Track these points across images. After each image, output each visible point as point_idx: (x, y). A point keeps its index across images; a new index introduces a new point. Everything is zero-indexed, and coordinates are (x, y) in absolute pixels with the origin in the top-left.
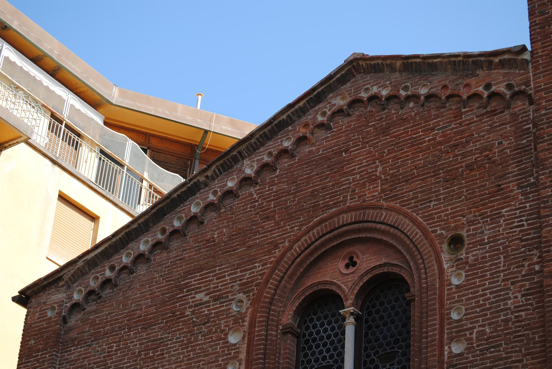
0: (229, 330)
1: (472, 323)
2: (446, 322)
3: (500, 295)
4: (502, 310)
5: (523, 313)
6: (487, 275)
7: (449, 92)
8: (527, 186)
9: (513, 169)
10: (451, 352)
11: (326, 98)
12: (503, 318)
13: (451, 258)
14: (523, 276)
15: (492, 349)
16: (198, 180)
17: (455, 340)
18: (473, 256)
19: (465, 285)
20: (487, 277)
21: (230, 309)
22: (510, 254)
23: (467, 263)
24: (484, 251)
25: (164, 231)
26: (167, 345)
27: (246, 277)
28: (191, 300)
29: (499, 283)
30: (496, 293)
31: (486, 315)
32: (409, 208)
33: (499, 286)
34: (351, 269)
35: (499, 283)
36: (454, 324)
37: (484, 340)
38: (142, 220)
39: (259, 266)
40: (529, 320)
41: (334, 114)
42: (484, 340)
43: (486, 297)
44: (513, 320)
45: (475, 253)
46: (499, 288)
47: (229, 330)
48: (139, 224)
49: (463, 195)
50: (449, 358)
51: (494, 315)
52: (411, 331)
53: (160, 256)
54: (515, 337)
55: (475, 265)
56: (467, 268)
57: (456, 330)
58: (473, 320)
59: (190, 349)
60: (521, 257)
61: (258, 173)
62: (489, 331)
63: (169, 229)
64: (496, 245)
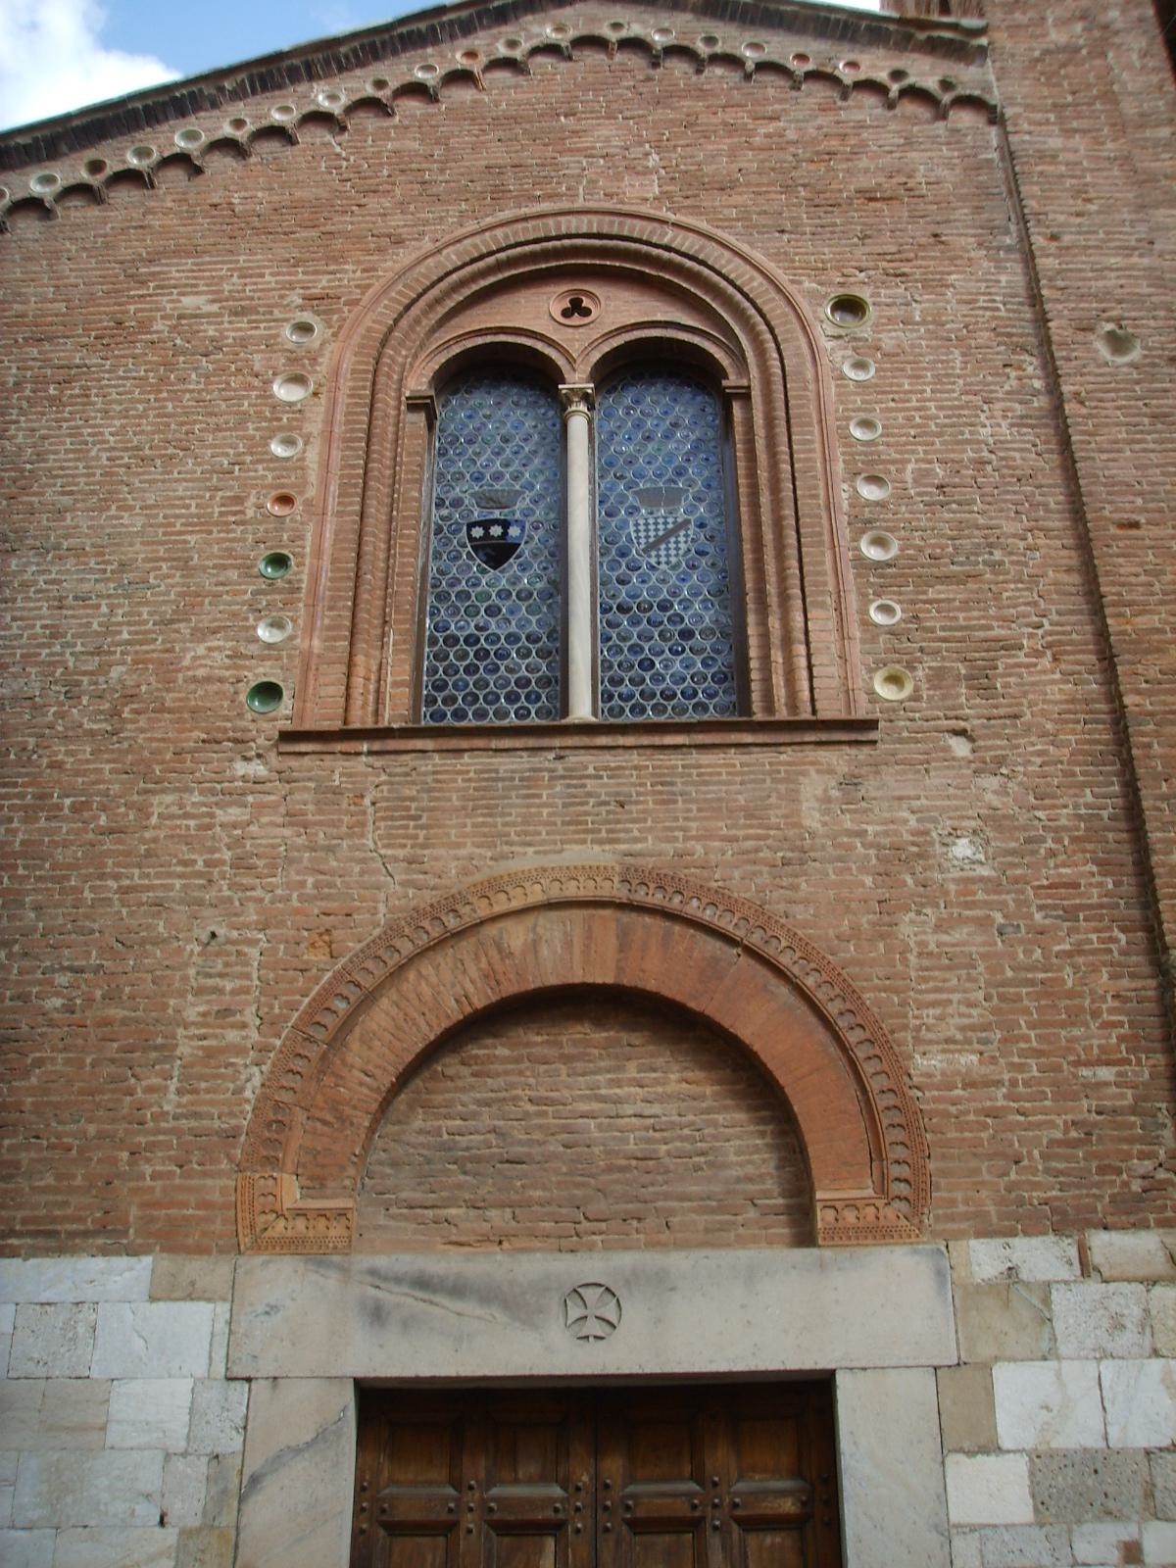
0: (275, 374)
1: (901, 453)
3: (960, 416)
4: (968, 442)
7: (810, 66)
8: (999, 249)
9: (963, 213)
11: (517, 18)
14: (1008, 393)
16: (200, 90)
18: (891, 338)
19: (876, 385)
21: (278, 335)
23: (878, 349)
25: (96, 167)
26: (99, 380)
28: (169, 306)
33: (956, 399)
34: (576, 320)
38: (47, 132)
39: (354, 272)
41: (536, 51)
42: (932, 485)
47: (275, 374)
48: (36, 140)
53: (77, 211)
55: (898, 355)
59: (165, 395)
61: (350, 110)
63: (112, 167)
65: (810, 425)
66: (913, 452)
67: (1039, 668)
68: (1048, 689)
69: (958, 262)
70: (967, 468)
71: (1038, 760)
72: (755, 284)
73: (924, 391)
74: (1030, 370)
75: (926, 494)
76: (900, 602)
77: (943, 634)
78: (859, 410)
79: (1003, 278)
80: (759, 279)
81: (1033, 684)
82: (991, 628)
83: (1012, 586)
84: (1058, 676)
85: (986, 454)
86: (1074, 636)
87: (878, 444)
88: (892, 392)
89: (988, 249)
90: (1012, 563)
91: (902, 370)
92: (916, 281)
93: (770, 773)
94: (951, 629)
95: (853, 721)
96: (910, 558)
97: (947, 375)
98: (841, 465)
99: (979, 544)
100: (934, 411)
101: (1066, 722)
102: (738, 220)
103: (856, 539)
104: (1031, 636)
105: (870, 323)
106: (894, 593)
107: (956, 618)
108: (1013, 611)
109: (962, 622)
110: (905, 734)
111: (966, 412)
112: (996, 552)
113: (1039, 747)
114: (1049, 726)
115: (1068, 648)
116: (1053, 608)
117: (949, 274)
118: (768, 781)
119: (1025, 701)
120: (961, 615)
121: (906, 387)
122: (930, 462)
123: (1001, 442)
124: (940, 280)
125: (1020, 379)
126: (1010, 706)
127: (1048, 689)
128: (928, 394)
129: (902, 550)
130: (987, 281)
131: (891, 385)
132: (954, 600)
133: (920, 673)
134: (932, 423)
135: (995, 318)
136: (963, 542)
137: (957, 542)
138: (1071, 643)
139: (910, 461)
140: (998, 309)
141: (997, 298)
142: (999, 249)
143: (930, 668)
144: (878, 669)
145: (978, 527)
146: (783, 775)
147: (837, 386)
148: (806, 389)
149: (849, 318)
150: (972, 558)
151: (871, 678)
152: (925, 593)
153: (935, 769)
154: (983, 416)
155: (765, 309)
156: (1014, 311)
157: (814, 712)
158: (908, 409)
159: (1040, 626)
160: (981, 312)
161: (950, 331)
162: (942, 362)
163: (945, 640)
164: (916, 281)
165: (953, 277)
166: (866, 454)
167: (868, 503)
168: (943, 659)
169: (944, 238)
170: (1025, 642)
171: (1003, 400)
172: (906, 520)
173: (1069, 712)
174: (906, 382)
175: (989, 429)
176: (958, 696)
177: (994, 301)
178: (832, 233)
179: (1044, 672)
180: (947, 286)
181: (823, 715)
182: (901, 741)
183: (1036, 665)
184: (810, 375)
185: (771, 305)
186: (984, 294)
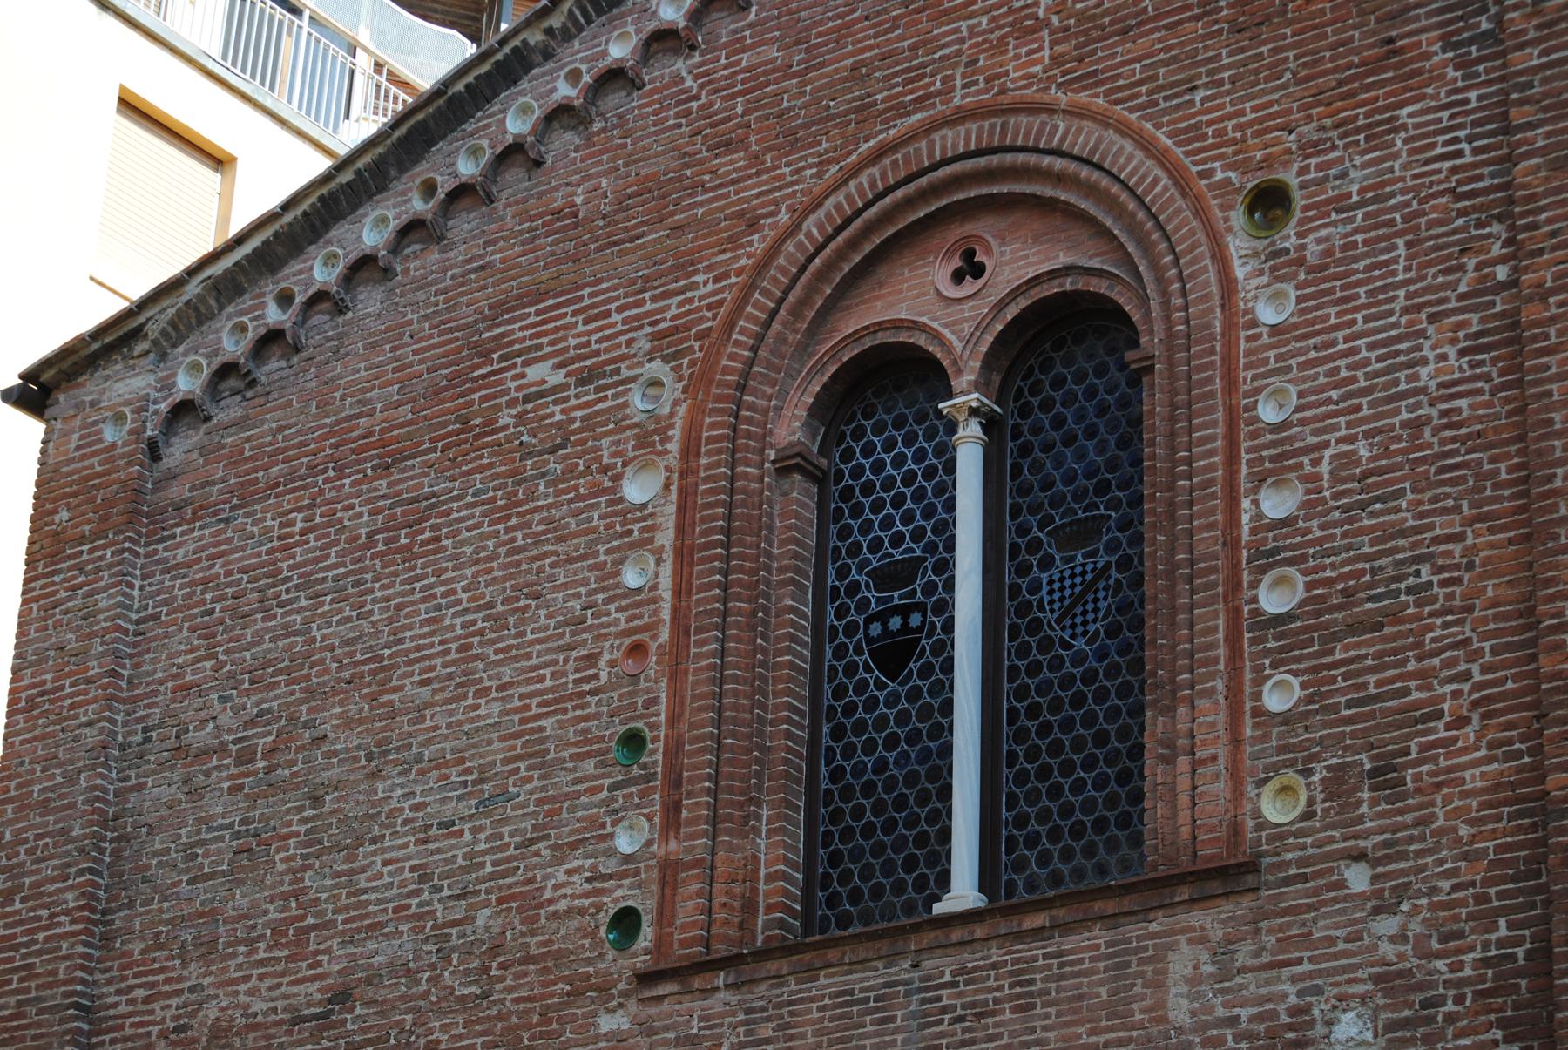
3: (1397, 353)
4: (1403, 395)
8: (1471, 41)
10: (1259, 516)
14: (1462, 297)
17: (1270, 480)
23: (1300, 262)
24: (1349, 228)
30: (1385, 346)
31: (1358, 408)
32: (1131, 110)
44: (1435, 422)
45: (1323, 233)
46: (1393, 333)
50: (1253, 531)
54: (1441, 470)
56: (1302, 276)
57: (1272, 452)
67: (1460, 744)
71: (1446, 885)
76: (1295, 673)
83: (1439, 621)
86: (1510, 685)
119: (1439, 799)
127: (1467, 775)
132: (1365, 657)
133: (1316, 778)
137: (1377, 564)
138: (1503, 696)
139: (1326, 444)
143: (1328, 768)
146: (1150, 952)
151: (1258, 795)
170: (1446, 706)
175: (1432, 367)
176: (1360, 803)
182: (1288, 881)
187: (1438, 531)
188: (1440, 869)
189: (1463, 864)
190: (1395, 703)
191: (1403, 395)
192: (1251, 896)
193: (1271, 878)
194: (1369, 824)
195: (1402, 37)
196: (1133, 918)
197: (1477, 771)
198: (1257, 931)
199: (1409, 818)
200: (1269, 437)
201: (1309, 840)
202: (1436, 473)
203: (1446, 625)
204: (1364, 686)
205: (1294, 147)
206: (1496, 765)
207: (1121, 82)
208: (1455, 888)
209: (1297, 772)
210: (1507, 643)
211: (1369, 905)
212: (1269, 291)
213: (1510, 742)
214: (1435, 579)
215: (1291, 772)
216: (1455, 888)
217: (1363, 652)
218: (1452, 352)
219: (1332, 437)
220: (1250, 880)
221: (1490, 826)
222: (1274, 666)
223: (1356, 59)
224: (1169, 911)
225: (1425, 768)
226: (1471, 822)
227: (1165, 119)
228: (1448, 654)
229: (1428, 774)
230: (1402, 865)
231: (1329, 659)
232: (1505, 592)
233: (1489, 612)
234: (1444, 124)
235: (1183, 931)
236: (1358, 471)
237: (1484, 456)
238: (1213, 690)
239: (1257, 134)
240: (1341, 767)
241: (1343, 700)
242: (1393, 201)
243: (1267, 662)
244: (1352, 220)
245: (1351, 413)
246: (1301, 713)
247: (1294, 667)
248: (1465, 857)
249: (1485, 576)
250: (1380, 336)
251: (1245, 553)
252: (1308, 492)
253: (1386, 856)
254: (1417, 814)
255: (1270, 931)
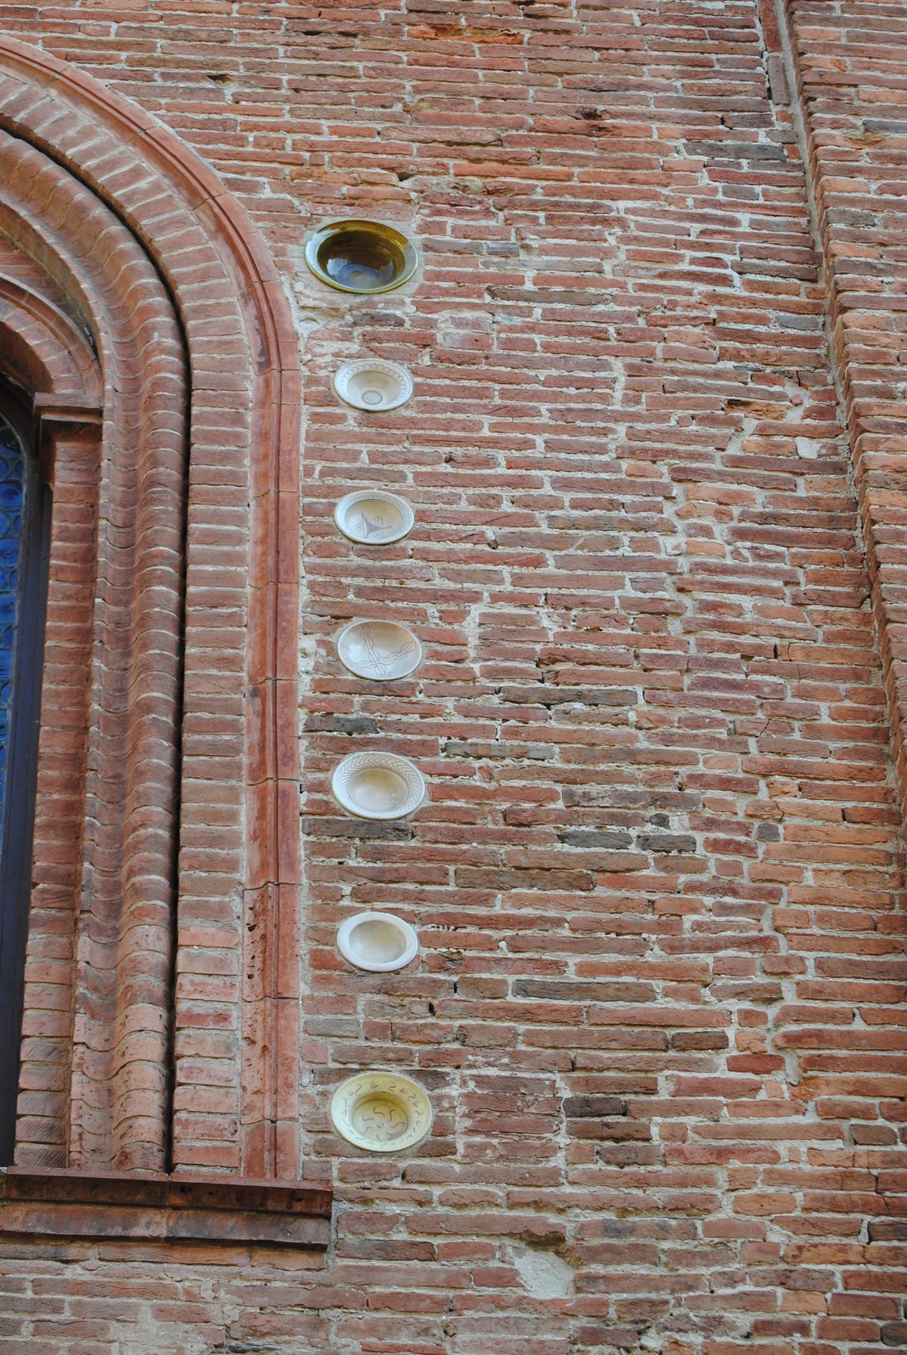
2: (302, 541)
3: (613, 505)
4: (626, 564)
5: (747, 602)
6: (493, 427)
8: (740, 152)
10: (334, 663)
12: (630, 592)
13: (333, 302)
14: (736, 462)
15: (578, 706)
17: (356, 621)
18: (460, 324)
20: (536, 421)
22: (658, 364)
23: (425, 343)
24: (517, 321)
27: (415, 30)
29: (605, 458)
30: (590, 489)
31: (538, 562)
32: (97, 73)
33: (605, 467)
35: (605, 458)
36: (353, 557)
37: (529, 659)
40: (782, 637)
42: (528, 656)
43: (535, 492)
44: (689, 614)
45: (468, 315)
46: (604, 476)
49: (400, 100)
50: (321, 687)
51: (579, 572)
52: (52, 552)
54: (706, 684)
55: (473, 360)
56: (426, 361)
57: (360, 581)
58: (464, 567)
60: (720, 390)
62: (557, 629)
64: (582, 313)
65: (237, 499)
66: (488, 577)
67: (762, 1095)
68: (782, 1147)
69: (639, 173)
70: (620, 622)
71: (745, 1320)
72: (143, 184)
73: (531, 444)
74: (794, 417)
75: (509, 673)
76: (411, 918)
77: (521, 1000)
78: (362, 473)
79: (745, 218)
80: (155, 175)
81: (743, 1133)
82: (647, 995)
83: (709, 901)
84: (810, 1119)
85: (668, 594)
86: (859, 1025)
87: (401, 554)
88: (448, 442)
89: (712, 150)
90: (716, 846)
91: (480, 394)
92: (535, 206)
93: (34, 1307)
94: (544, 991)
95: (266, 1192)
96: (451, 815)
97: (588, 414)
98: (304, 595)
99: (633, 798)
100: (548, 489)
101: (821, 1228)
102: (120, 46)
103: (323, 765)
104: (748, 1017)
105: (412, 288)
106: (406, 896)
107: (557, 967)
108: (707, 959)
109: (572, 976)
110: (401, 1235)
111: (627, 499)
112: (674, 820)
113: (748, 1287)
114: (777, 1236)
115: (843, 1053)
116: (810, 957)
117: (615, 196)
118: (26, 1330)
119: (721, 1175)
120: (573, 960)
121: (486, 432)
122: (526, 602)
123: (709, 569)
124: (592, 208)
125: (762, 432)
126: (682, 1183)
127: (782, 1147)
128: (539, 451)
129: (437, 793)
130: (703, 218)
131: (448, 425)
132: (558, 922)
133: (454, 1091)
134: (540, 515)
135: (715, 298)
136: (593, 788)
137: (579, 789)
138: (850, 1040)
139: (475, 597)
140: (725, 281)
141: (727, 258)
142: (740, 152)
143: (481, 1081)
144: (342, 1075)
145: (633, 757)
146: (67, 1315)
147: (315, 418)
148: (238, 420)
149: (364, 281)
150: (614, 829)
151: (324, 1095)
152: (486, 900)
153: (471, 1326)
154: (669, 510)
155: (159, 240)
156: (765, 288)
157: (169, 1166)
158: (485, 482)
159: (772, 997)
160: (685, 284)
161: (608, 317)
162: (579, 383)
163: (527, 1015)
164: (535, 206)
165: (622, 204)
166: (368, 573)
167: (363, 686)
168: (516, 1057)
169: (609, 122)
170: (731, 1032)
171: (721, 476)
172: (449, 730)
173: (835, 1207)
174: (487, 420)
175: (681, 539)
176: (549, 1151)
177: (718, 262)
178: (343, 89)
179: (776, 1107)
180: (606, 222)
181: (185, 1173)
182: (388, 1251)
183: (754, 1089)
184: (251, 389)
185: (175, 233)
186: (692, 246)
187: (701, 769)
188: (729, 1291)
189: (780, 1291)
190: (620, 1006)
191: (626, 564)
192: (305, 1260)
193: (350, 1238)
194: (568, 1189)
195: (614, 116)
196: (28, 1249)
197: (802, 1146)
198: (319, 1325)
199: (658, 1195)
200: (356, 560)
201: (437, 1192)
202: (693, 686)
203: (724, 909)
204: (557, 967)
205: (413, 195)
206: (839, 1144)
207: (80, 36)
208: (760, 1328)
209: (410, 1073)
210: (850, 962)
211: (573, 1324)
212: (360, 365)
213: (866, 1113)
214: (700, 837)
215: (396, 1071)
216: (760, 1328)
217: (552, 913)
218: (721, 531)
219: (486, 590)
220: (309, 1231)
221: (833, 1240)
222: (363, 897)
223: (531, 121)
224: (112, 1251)
225: (691, 1121)
226: (795, 1226)
227: (163, 101)
228: (731, 952)
229: (696, 1130)
230: (642, 1270)
231: (481, 911)
232: (836, 885)
233: (811, 908)
234: (692, 238)
235: (144, 1292)
236: (538, 647)
237: (791, 685)
238: (222, 910)
239: (344, 163)
240: (512, 1085)
241: (511, 979)
242: (601, 308)
243: (347, 889)
244: (529, 312)
245: (522, 564)
246: (422, 981)
247: (407, 907)
248: (783, 1280)
249: (797, 852)
250: (579, 475)
251: (302, 716)
252: (436, 655)
253: (609, 1249)
254: (675, 1191)
255: (346, 1329)
